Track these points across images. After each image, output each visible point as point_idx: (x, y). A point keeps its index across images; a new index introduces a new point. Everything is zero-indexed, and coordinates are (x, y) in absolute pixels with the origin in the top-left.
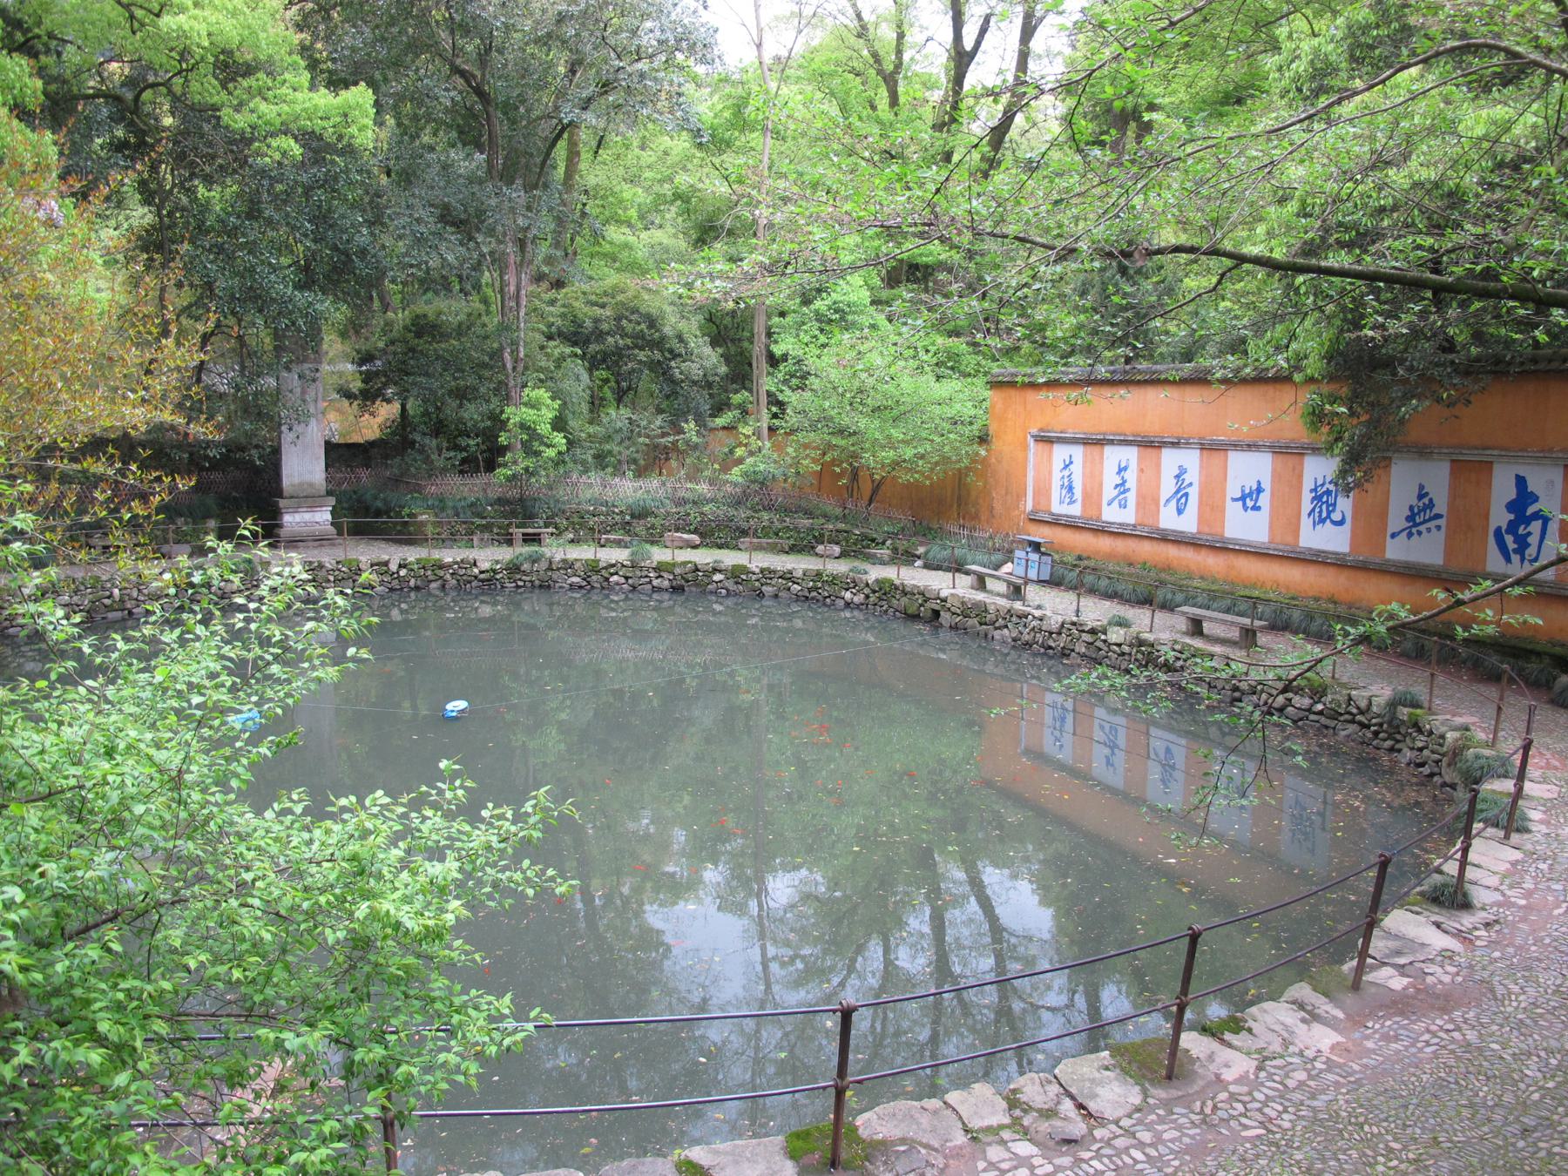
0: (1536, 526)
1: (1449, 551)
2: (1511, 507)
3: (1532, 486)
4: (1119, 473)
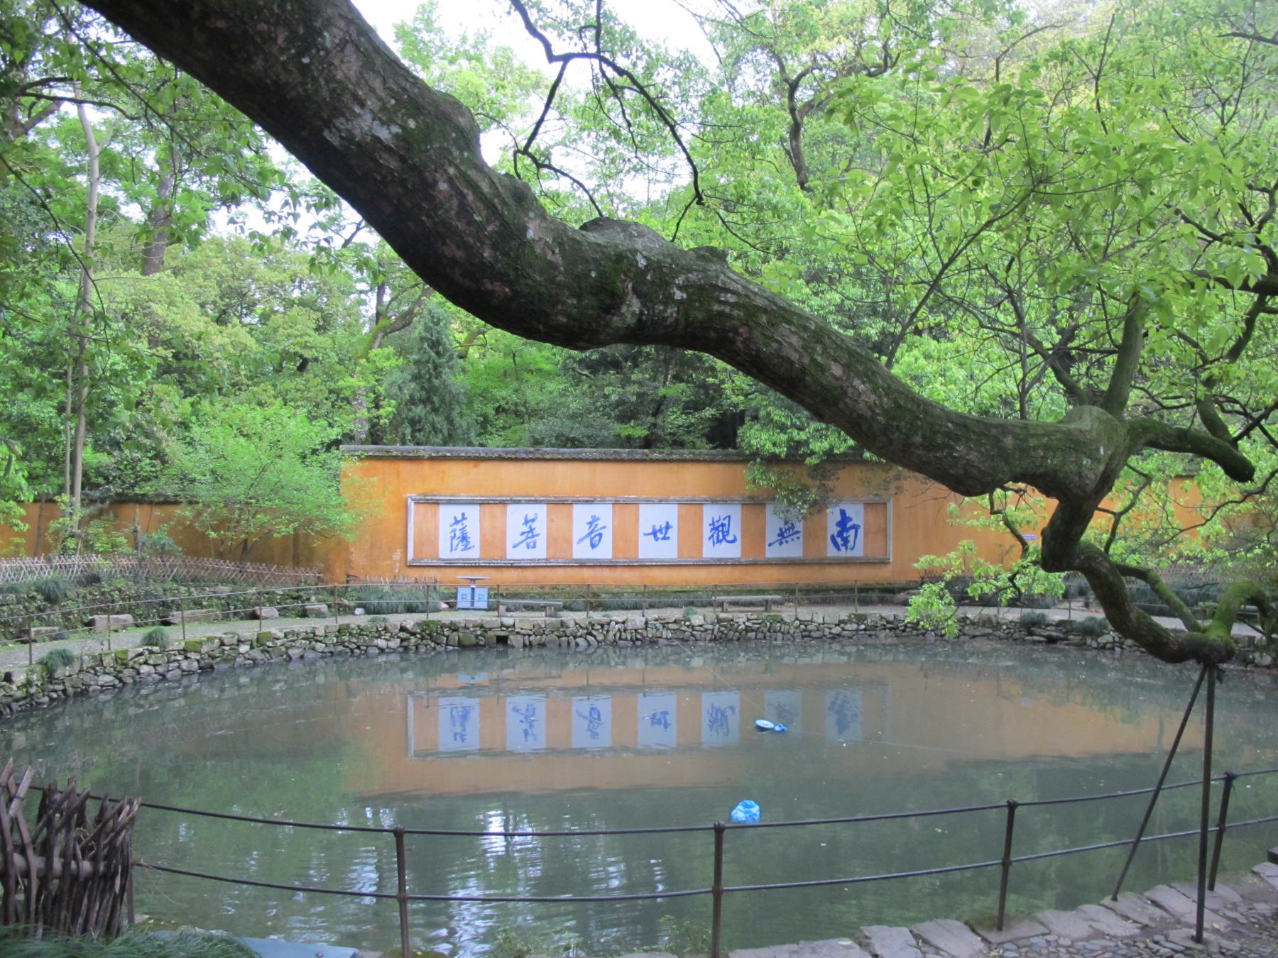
0: (852, 532)
1: (805, 550)
2: (838, 524)
3: (848, 514)
4: (526, 522)
